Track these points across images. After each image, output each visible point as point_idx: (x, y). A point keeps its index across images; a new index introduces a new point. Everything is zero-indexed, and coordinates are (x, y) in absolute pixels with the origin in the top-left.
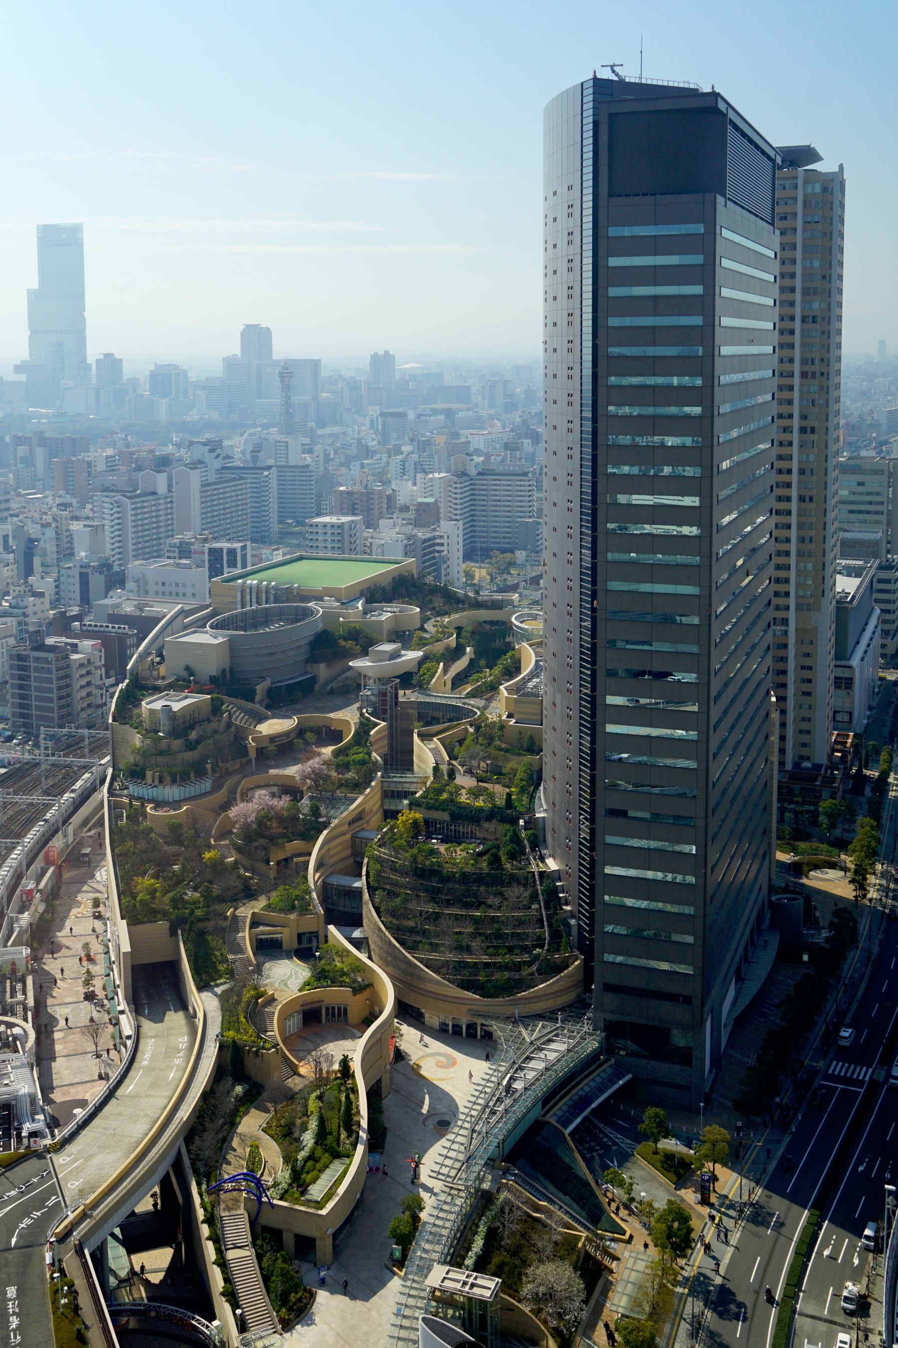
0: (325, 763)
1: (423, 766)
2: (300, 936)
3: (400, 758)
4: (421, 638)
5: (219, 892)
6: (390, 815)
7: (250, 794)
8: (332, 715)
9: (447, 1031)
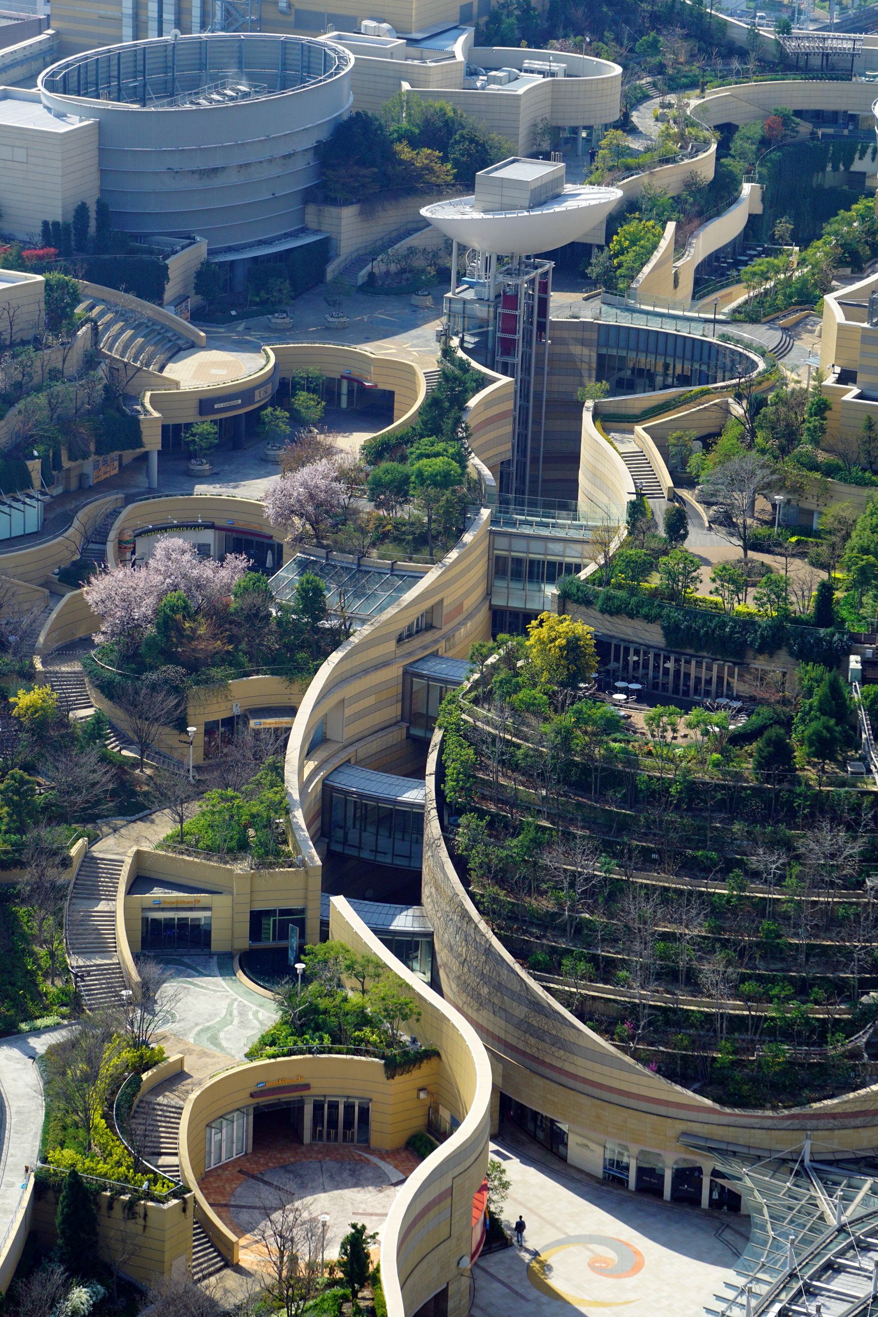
0: (343, 476)
1: (603, 499)
2: (257, 918)
3: (544, 474)
4: (621, 152)
5: (52, 795)
6: (509, 622)
7: (141, 545)
8: (368, 349)
9: (622, 1183)
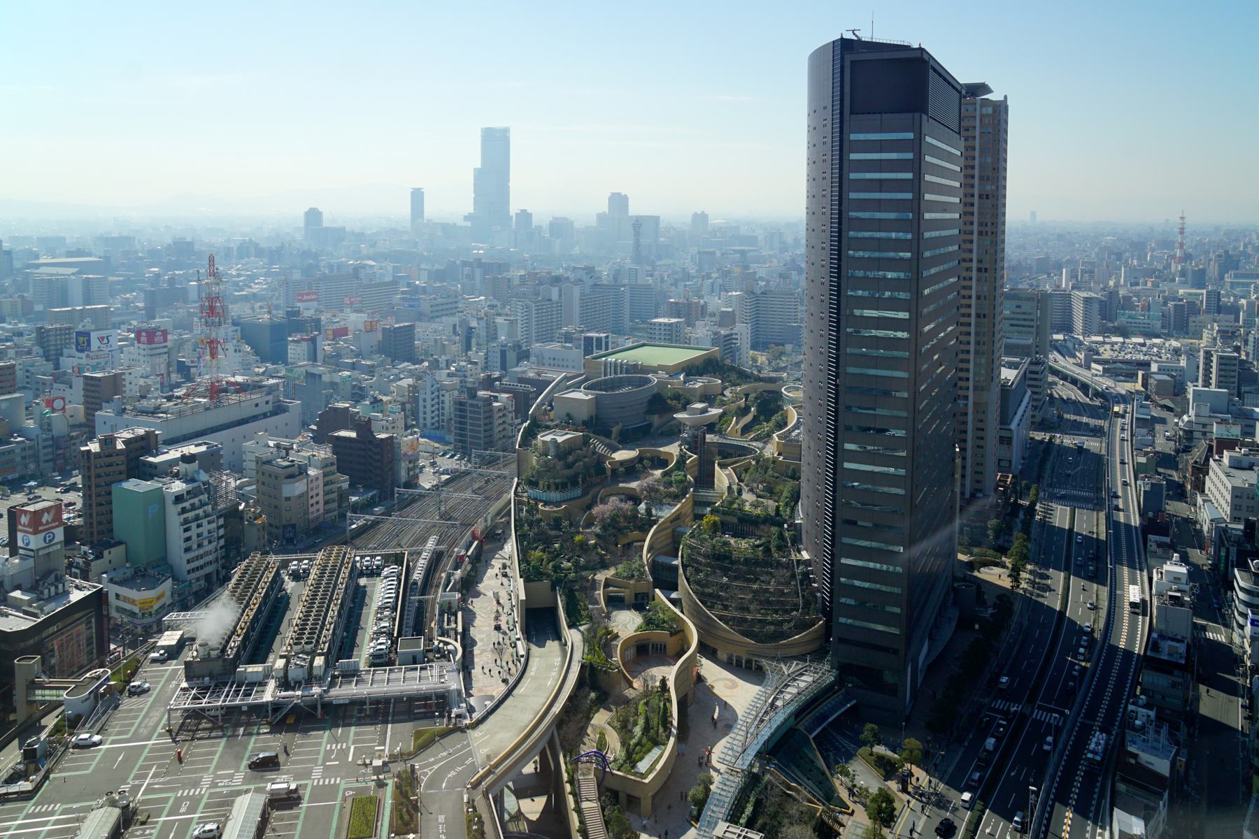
2: (636, 595)
3: (705, 479)
